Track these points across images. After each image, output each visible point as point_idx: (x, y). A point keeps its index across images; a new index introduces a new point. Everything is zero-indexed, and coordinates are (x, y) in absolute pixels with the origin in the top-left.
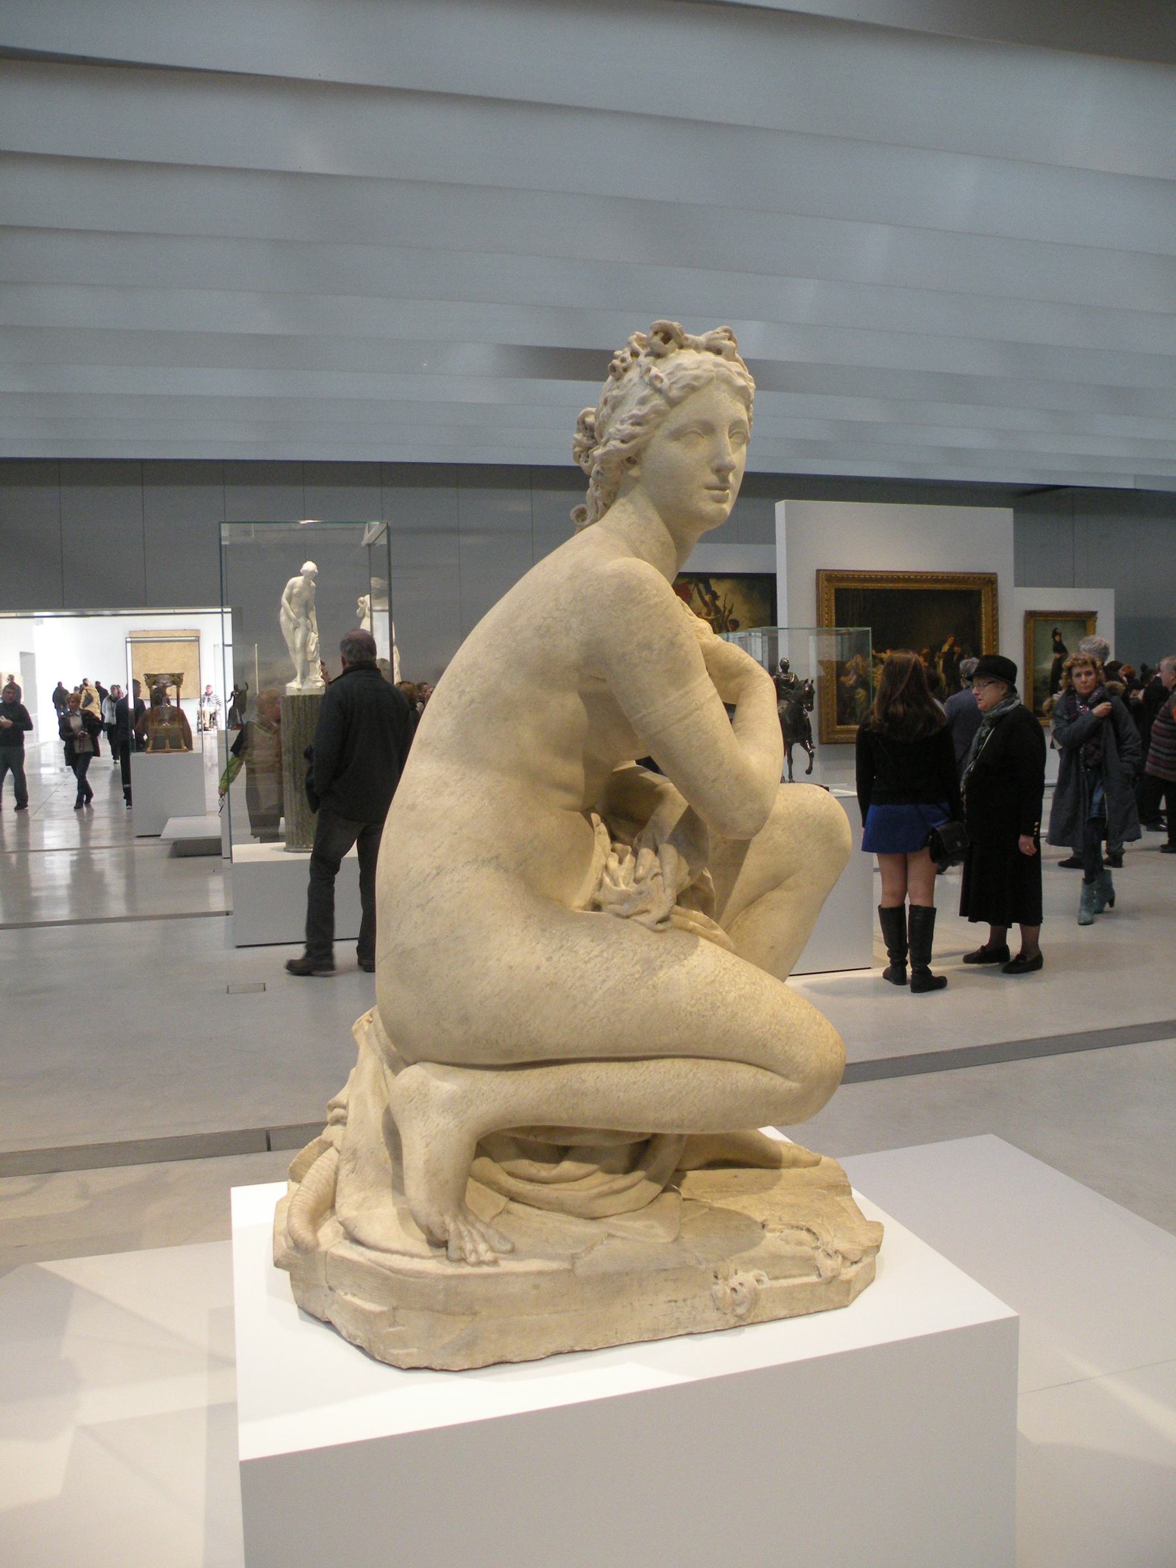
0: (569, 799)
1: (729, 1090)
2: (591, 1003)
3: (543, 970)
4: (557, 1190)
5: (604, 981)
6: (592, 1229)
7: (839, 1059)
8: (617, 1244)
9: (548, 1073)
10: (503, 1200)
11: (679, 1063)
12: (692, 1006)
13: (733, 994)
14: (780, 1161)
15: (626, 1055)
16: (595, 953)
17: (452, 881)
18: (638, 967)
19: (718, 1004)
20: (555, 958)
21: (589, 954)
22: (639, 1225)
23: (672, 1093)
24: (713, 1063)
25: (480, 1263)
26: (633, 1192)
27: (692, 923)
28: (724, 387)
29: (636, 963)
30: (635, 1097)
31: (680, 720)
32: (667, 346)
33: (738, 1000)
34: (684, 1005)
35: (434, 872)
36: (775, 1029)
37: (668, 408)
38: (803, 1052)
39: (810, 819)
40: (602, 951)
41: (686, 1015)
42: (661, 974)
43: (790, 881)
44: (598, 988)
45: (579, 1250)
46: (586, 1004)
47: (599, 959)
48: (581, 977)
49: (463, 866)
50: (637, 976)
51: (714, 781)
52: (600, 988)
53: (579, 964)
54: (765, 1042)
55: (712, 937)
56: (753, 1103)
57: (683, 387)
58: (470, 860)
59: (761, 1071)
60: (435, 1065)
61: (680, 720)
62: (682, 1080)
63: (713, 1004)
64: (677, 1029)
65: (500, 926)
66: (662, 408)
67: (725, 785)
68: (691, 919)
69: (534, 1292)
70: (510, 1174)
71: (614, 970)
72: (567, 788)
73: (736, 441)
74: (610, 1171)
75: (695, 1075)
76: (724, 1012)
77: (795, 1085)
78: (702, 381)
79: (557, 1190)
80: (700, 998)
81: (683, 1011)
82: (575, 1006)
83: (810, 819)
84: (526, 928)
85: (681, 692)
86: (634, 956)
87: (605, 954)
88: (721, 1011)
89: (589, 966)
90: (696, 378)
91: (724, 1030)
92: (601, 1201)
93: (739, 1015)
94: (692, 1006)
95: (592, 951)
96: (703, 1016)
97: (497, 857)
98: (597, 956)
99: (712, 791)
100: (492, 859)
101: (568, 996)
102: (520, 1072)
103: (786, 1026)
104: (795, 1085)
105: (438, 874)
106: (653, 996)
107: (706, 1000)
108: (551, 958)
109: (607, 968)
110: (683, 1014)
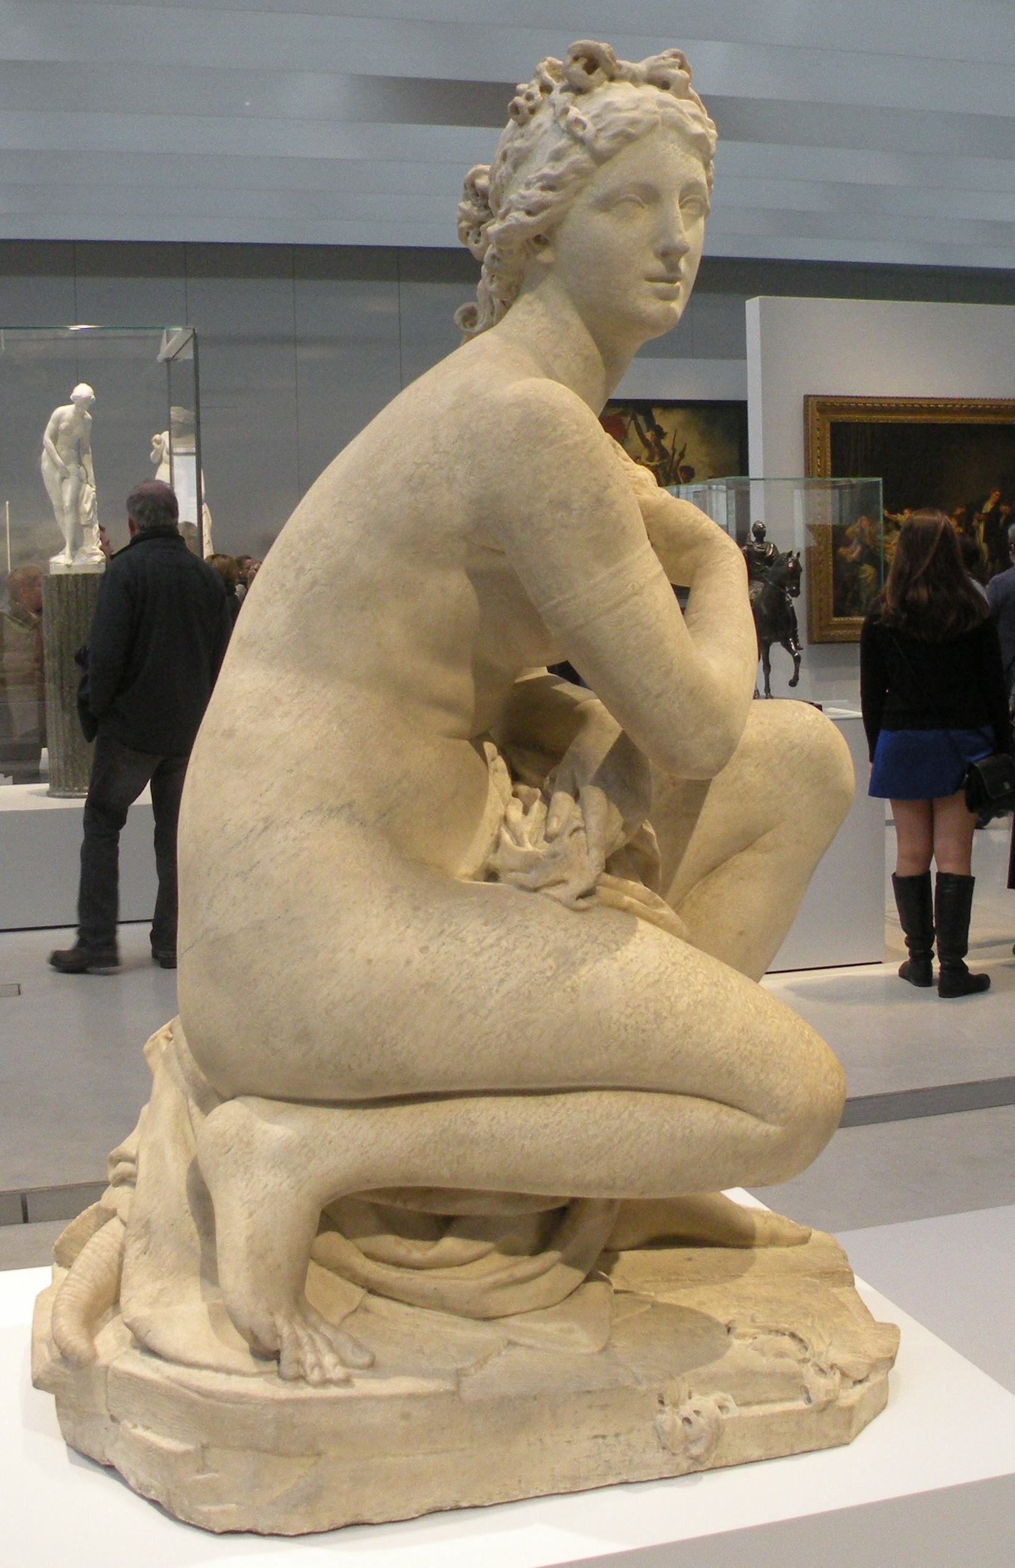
1: (679, 1135)
2: (483, 1012)
5: (502, 981)
8: (520, 1355)
10: (358, 1294)
11: (608, 1097)
17: (286, 838)
18: (550, 961)
20: (433, 949)
25: (326, 1382)
26: (543, 1282)
29: (548, 956)
35: (261, 826)
40: (500, 939)
43: (767, 838)
44: (494, 991)
45: (467, 1364)
47: (495, 949)
48: (470, 976)
50: (549, 974)
51: (658, 696)
52: (497, 991)
55: (655, 918)
59: (725, 1108)
65: (354, 903)
68: (627, 894)
69: (403, 1423)
72: (448, 706)
74: (511, 1251)
81: (615, 1024)
82: (461, 1017)
83: (796, 751)
85: (612, 569)
87: (504, 943)
88: (668, 1024)
89: (481, 959)
97: (350, 805)
98: (492, 946)
104: (773, 1129)
105: (266, 828)
106: (572, 1002)
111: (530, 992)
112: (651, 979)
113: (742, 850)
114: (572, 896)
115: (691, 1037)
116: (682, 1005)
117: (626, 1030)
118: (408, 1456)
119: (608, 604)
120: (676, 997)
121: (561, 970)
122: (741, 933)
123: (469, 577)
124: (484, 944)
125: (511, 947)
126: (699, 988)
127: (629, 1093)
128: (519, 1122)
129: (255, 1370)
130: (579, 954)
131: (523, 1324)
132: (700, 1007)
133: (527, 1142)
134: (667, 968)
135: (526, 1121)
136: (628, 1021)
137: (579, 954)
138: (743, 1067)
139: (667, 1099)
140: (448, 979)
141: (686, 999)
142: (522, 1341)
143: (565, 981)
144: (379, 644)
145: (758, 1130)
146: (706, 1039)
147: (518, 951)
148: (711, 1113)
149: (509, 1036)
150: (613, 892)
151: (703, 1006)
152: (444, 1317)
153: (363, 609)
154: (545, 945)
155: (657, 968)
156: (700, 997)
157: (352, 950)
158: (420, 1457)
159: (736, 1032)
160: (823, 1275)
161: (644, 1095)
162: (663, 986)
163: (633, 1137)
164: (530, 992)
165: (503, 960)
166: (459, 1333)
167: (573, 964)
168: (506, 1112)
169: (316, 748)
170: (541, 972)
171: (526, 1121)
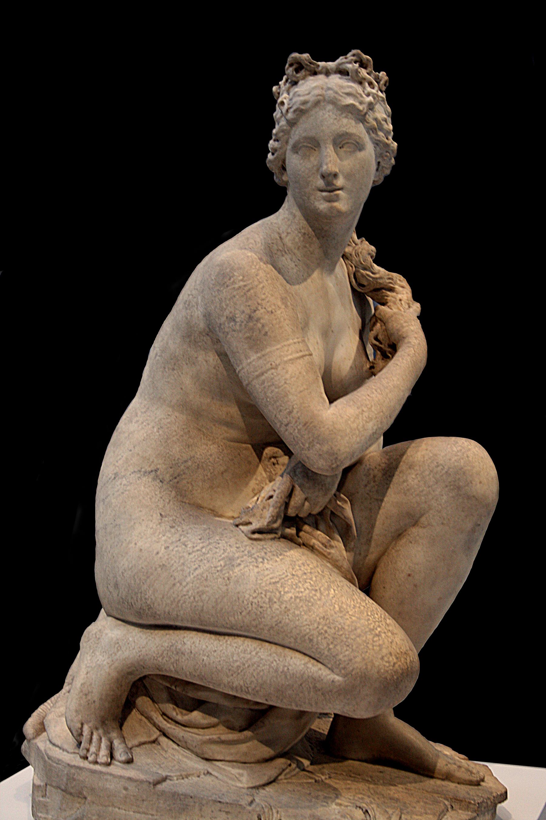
0: (234, 433)
1: (281, 670)
2: (184, 584)
3: (160, 555)
4: (189, 732)
5: (196, 569)
6: (202, 766)
7: (391, 668)
8: (208, 779)
9: (167, 634)
10: (156, 734)
11: (248, 642)
12: (253, 598)
13: (290, 595)
14: (433, 772)
15: (211, 628)
16: (198, 548)
17: (121, 484)
18: (222, 563)
19: (275, 600)
20: (171, 548)
21: (194, 547)
22: (235, 771)
23: (238, 663)
24: (274, 647)
25: (96, 762)
26: (243, 747)
27: (314, 541)
28: (330, 107)
29: (222, 559)
30: (214, 662)
31: (258, 376)
32: (298, 75)
33: (293, 600)
34: (247, 596)
35: (113, 477)
36: (322, 629)
37: (289, 128)
38: (347, 653)
39: (439, 469)
40: (203, 548)
41: (248, 604)
42: (236, 570)
43: (423, 519)
44: (191, 574)
45: (172, 774)
46: (181, 584)
47: (199, 552)
48: (183, 564)
49: (130, 475)
50: (219, 569)
51: (286, 425)
52: (193, 574)
53: (185, 554)
54: (311, 638)
55: (326, 554)
56: (301, 685)
57: (295, 111)
58: (136, 470)
59: (313, 661)
60: (114, 619)
61: (258, 376)
62: (246, 655)
63: (270, 600)
64: (241, 613)
65: (143, 520)
66: (285, 128)
67: (295, 429)
68: (315, 538)
69: (124, 792)
70: (164, 714)
71: (205, 562)
72: (229, 424)
73: (348, 150)
74: (231, 728)
75: (257, 653)
76: (279, 607)
77: (337, 678)
78: (309, 105)
79: (189, 732)
80: (261, 593)
81: (246, 600)
82: (174, 585)
83: (439, 469)
84: (160, 523)
85: (259, 355)
86: (223, 553)
87: (204, 550)
88: (276, 606)
89: (191, 556)
90: (305, 103)
91: (277, 621)
92: (214, 747)
93: (291, 612)
94: (253, 598)
95: (196, 546)
96: (261, 607)
97: (156, 471)
98: (198, 550)
99: (287, 433)
100: (152, 471)
101: (171, 576)
102: (152, 631)
103: (335, 629)
104: (337, 678)
105: (115, 478)
106: (226, 585)
107: (265, 596)
108: (168, 547)
109: (202, 559)
110: (245, 602)
111: (207, 576)
112: (273, 580)
113: (414, 525)
114: (249, 531)
115: (288, 615)
116: (287, 597)
117: (252, 604)
118: (125, 810)
119: (257, 373)
120: (285, 592)
121: (225, 568)
122: (409, 575)
123: (218, 356)
124: (196, 549)
125: (207, 552)
126: (303, 590)
127: (260, 642)
128: (204, 647)
129: (72, 751)
130: (239, 561)
131: (223, 767)
132: (298, 600)
133: (205, 658)
134: (287, 576)
135: (207, 647)
136: (253, 600)
137: (239, 561)
138: (320, 638)
139: (280, 649)
140: (173, 565)
141: (290, 595)
142: (213, 773)
143: (225, 574)
144: (182, 389)
145: (329, 677)
146: (297, 618)
147: (208, 555)
148: (303, 662)
149: (194, 598)
150: (308, 536)
151: (300, 600)
152: (188, 753)
153: (173, 369)
154: (223, 553)
155: (280, 575)
156: (301, 595)
157: (136, 544)
158: (131, 813)
159: (318, 618)
160: (453, 800)
161: (267, 644)
162: (279, 585)
163: (255, 666)
164: (207, 576)
165: (199, 559)
166: (188, 762)
167: (233, 566)
168: (200, 641)
169: (144, 440)
170: (215, 567)
171: (207, 647)
